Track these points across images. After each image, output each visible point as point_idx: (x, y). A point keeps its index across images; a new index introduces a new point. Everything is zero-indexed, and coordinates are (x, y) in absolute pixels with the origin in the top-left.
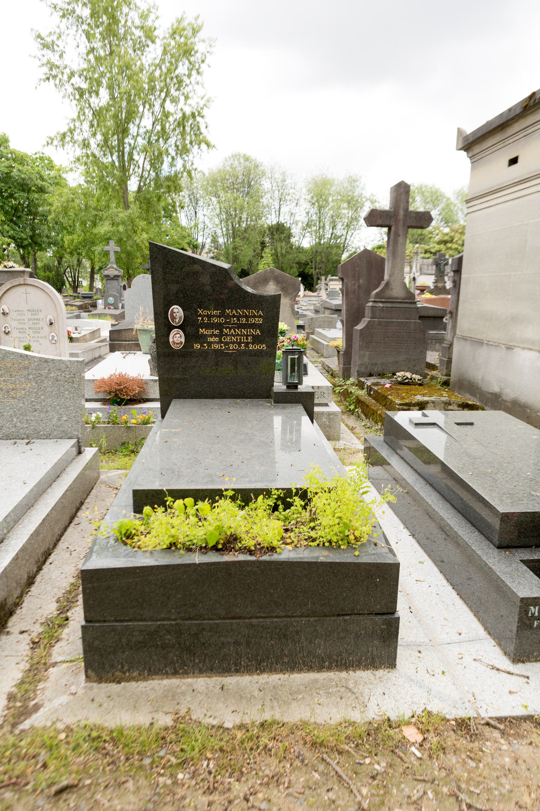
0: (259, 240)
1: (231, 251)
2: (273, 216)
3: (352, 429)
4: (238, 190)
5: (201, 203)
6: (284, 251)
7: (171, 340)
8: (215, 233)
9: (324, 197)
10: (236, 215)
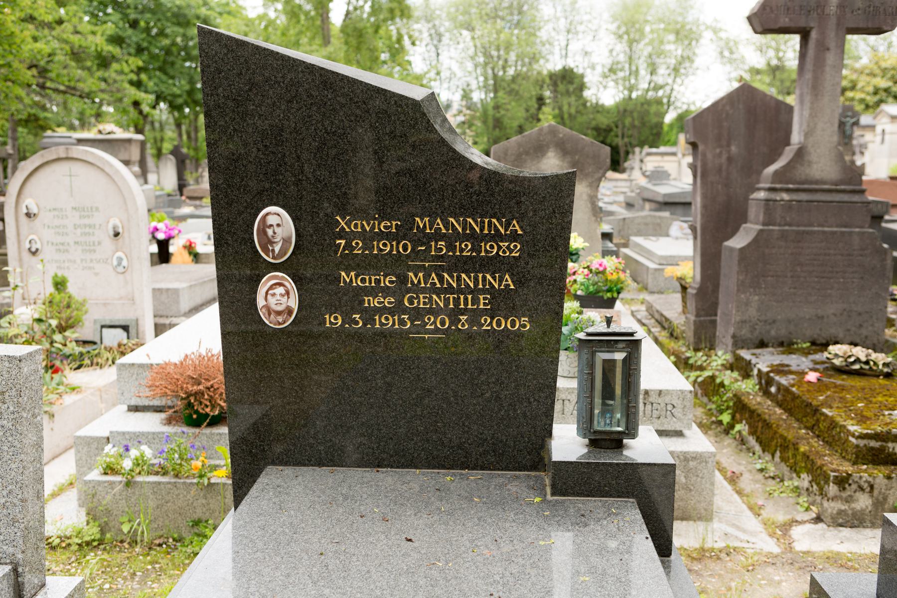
0: (534, 93)
1: (491, 112)
2: (557, 56)
3: (733, 479)
4: (503, 19)
5: (445, 40)
6: (573, 111)
7: (261, 302)
8: (468, 85)
9: (637, 26)
10: (499, 57)
